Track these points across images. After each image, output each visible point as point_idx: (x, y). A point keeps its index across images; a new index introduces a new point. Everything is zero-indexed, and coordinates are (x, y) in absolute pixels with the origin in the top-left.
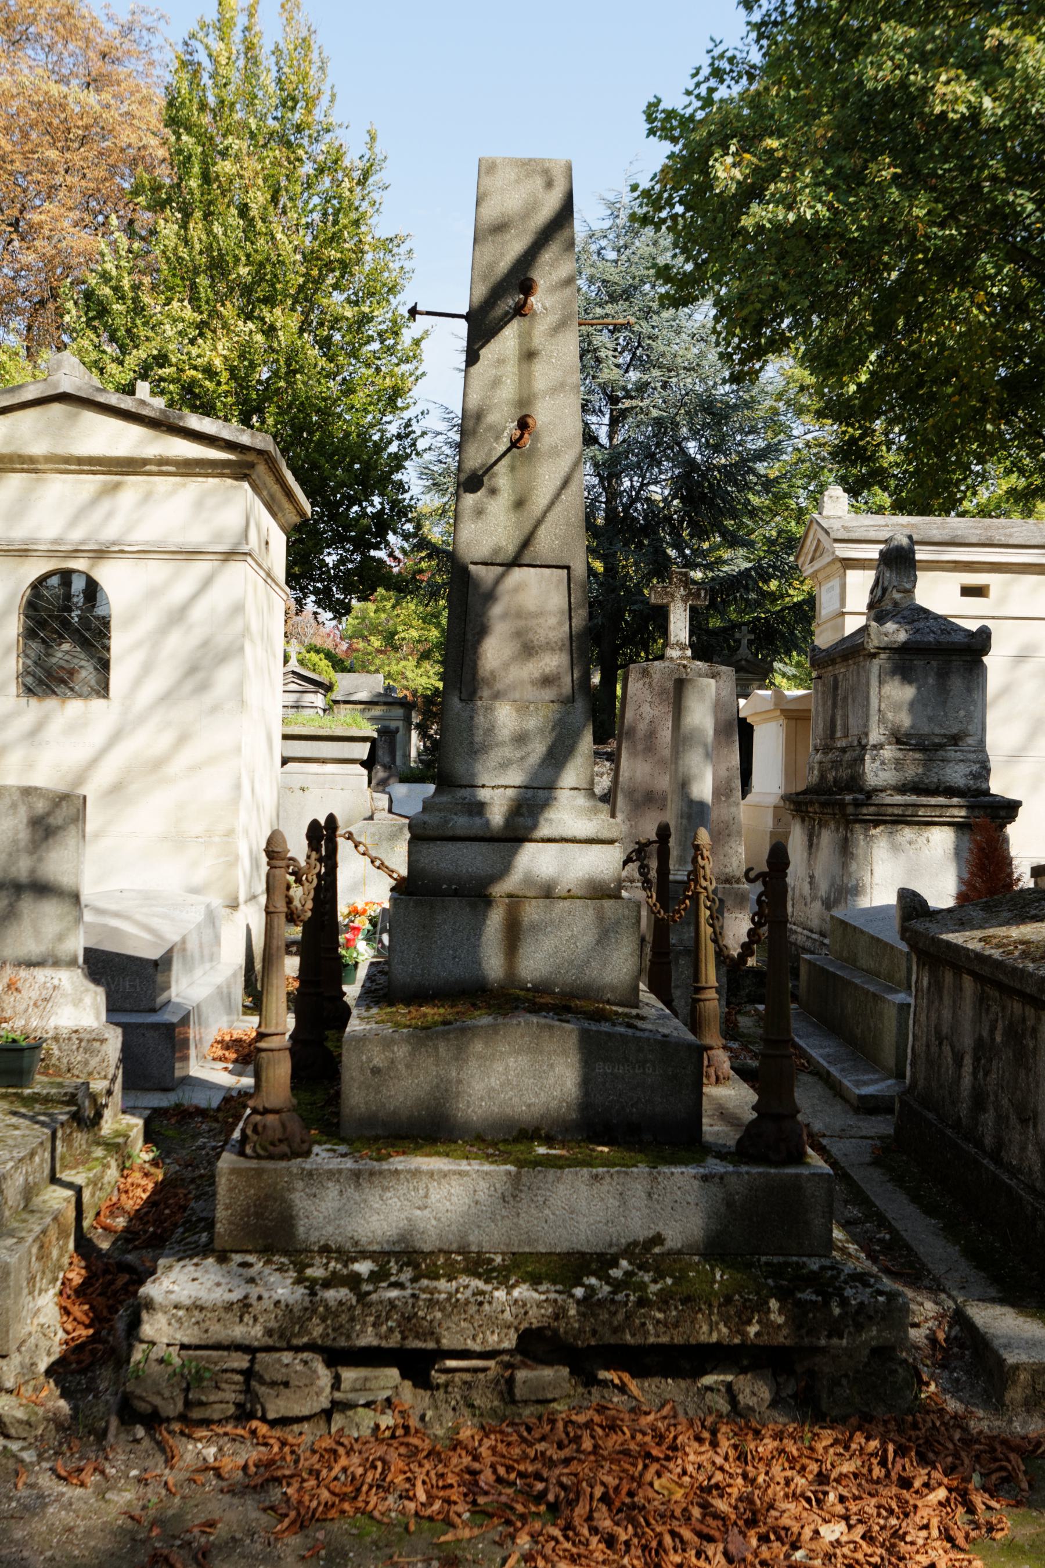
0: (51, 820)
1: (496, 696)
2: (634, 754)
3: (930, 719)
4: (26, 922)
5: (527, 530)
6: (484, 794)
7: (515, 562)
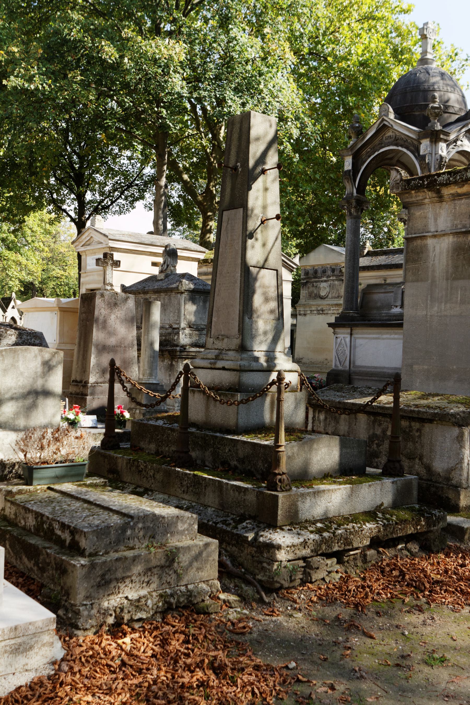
0: (51, 363)
1: (258, 317)
2: (98, 330)
3: (201, 319)
4: (40, 409)
5: (266, 255)
6: (256, 354)
7: (263, 267)
